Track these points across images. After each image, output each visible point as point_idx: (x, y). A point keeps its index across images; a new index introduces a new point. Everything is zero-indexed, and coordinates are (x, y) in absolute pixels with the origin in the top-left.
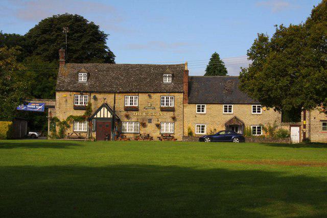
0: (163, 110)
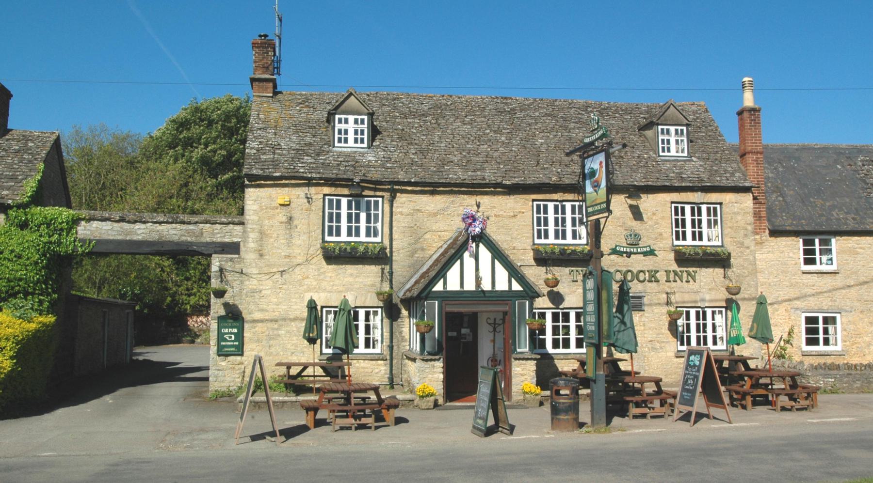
0: (684, 259)
